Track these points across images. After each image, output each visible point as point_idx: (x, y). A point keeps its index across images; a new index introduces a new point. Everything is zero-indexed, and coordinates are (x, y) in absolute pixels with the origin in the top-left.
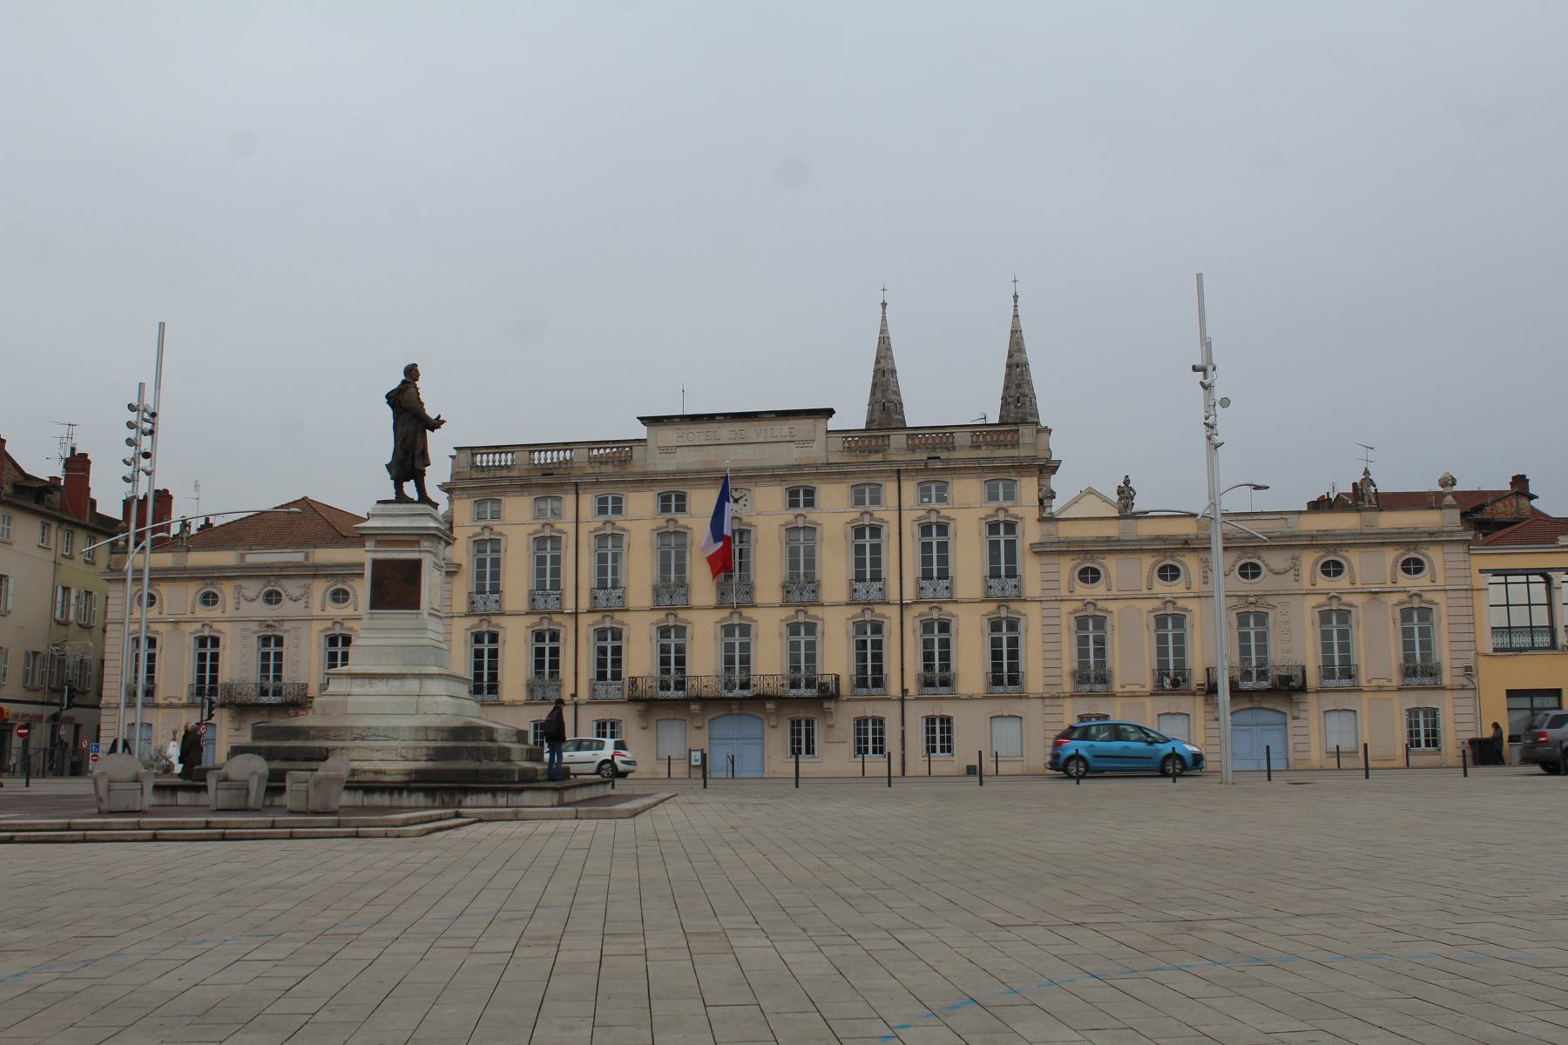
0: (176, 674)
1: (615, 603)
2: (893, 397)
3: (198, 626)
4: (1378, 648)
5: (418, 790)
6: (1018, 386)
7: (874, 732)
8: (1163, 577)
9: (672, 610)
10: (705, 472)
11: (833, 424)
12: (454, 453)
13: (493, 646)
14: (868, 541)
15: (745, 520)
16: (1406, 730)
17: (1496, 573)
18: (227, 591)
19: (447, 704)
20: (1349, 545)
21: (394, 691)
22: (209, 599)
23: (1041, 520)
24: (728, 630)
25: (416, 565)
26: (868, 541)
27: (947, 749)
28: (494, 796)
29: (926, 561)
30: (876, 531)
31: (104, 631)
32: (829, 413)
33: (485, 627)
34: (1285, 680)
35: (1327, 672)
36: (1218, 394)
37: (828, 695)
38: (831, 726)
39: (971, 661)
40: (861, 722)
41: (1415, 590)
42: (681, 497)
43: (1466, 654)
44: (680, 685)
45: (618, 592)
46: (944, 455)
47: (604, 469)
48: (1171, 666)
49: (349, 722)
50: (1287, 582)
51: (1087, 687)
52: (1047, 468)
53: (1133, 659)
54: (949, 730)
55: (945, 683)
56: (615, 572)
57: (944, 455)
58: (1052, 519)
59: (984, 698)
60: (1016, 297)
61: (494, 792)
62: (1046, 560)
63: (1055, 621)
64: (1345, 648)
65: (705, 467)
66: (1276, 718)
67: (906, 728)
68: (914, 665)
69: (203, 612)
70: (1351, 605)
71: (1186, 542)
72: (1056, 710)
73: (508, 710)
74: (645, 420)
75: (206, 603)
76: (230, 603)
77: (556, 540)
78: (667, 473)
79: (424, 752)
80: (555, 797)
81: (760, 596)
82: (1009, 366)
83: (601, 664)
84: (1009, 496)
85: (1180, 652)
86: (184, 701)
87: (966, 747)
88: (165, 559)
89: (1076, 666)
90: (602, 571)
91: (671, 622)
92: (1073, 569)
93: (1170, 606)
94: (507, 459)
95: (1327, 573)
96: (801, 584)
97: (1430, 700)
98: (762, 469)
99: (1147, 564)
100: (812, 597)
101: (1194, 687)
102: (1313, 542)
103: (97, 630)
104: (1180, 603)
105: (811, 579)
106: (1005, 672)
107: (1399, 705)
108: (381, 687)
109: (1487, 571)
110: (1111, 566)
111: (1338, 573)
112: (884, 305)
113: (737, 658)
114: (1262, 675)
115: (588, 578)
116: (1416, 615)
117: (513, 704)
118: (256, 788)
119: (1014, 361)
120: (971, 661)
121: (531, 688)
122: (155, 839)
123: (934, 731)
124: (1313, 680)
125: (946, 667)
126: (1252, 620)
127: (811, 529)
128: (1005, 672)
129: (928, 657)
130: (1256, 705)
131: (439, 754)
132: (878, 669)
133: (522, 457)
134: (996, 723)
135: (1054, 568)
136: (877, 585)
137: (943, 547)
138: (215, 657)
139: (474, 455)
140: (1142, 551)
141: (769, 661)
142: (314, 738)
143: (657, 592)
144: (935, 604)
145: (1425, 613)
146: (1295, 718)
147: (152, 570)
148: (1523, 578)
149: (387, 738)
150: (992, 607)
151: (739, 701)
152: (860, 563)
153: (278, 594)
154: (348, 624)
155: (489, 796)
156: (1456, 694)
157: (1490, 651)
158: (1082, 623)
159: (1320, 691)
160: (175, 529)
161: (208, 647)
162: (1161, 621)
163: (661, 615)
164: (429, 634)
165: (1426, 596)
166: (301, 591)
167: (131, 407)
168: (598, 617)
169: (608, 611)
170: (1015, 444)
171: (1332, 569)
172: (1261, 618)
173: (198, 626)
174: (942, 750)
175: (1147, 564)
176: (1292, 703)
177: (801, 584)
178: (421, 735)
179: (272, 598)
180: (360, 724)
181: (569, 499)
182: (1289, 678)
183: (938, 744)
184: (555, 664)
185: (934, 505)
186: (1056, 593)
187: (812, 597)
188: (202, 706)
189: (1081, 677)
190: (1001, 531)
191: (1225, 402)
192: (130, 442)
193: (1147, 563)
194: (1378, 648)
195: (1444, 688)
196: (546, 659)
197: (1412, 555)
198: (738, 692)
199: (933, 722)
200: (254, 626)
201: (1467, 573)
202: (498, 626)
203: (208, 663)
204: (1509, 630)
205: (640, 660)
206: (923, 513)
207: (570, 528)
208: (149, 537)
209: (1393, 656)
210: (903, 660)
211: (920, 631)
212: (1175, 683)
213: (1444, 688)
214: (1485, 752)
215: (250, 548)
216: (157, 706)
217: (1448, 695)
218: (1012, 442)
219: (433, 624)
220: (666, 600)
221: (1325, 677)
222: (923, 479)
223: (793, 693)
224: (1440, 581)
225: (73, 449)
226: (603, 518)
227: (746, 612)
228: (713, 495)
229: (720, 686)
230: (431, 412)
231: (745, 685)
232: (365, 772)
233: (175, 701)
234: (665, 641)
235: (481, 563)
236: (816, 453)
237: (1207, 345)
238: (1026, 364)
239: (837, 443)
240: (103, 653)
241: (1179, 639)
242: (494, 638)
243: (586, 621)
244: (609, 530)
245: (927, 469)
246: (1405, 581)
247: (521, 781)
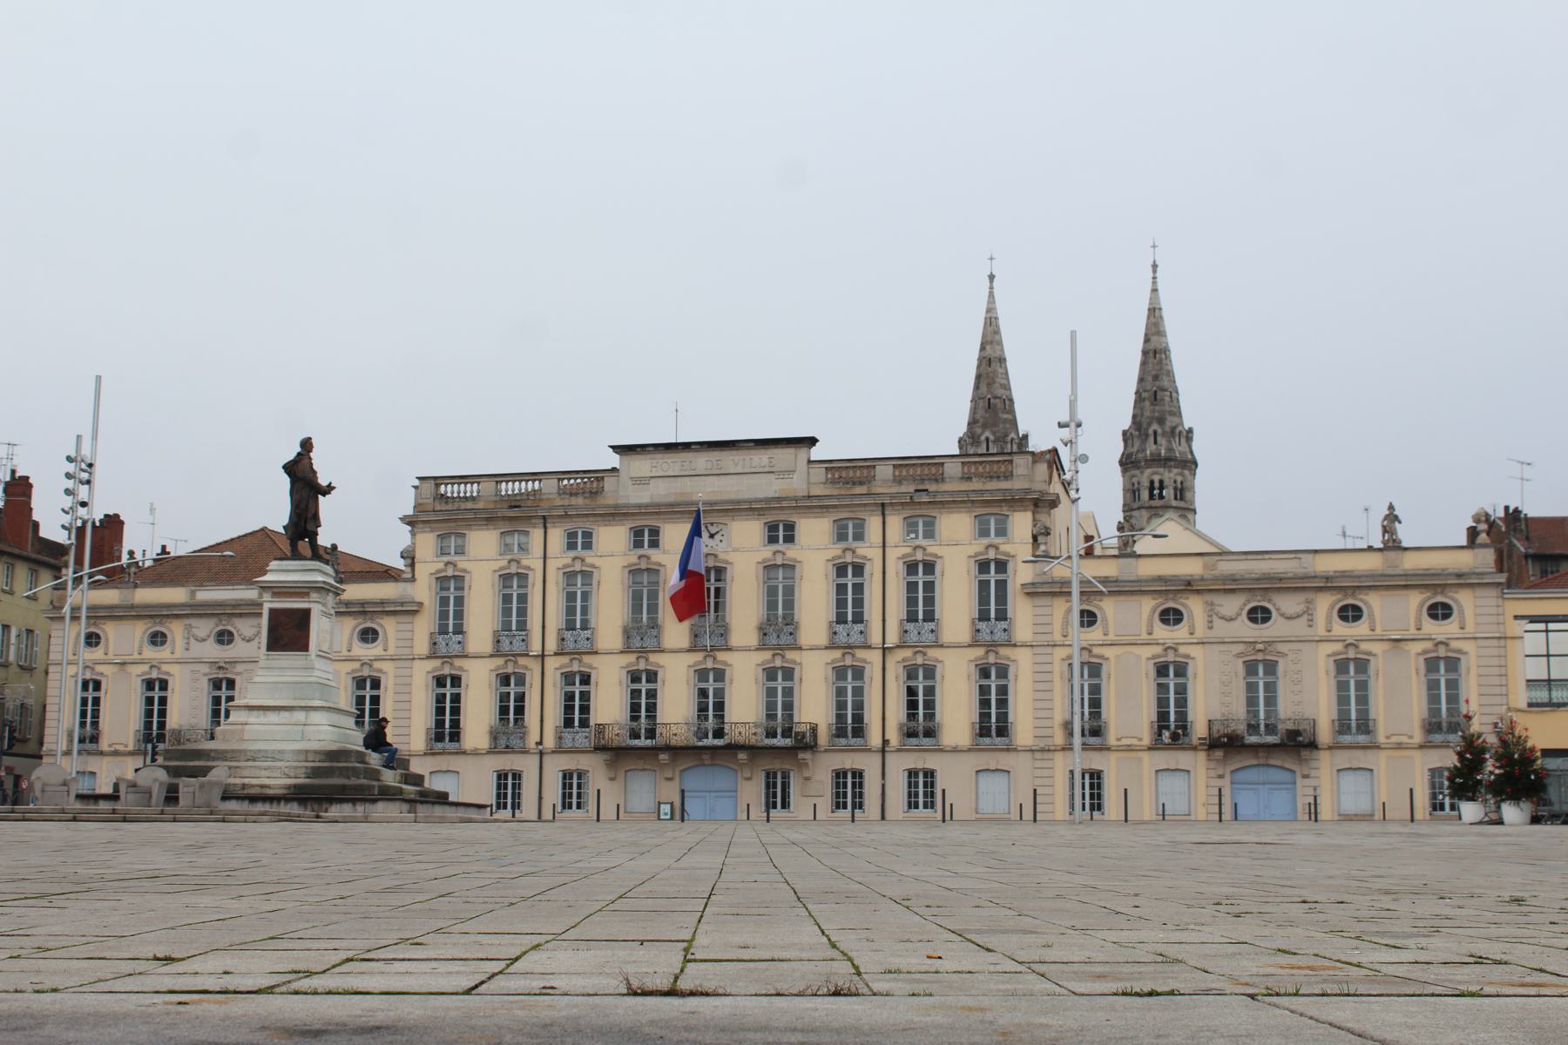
0: (122, 718)
2: (1000, 392)
3: (146, 668)
4: (1399, 703)
6: (1156, 378)
7: (925, 785)
9: (643, 652)
10: (678, 505)
11: (816, 453)
12: (417, 483)
14: (850, 580)
15: (722, 556)
17: (1534, 619)
18: (176, 630)
20: (1370, 588)
22: (158, 639)
25: (305, 615)
26: (850, 580)
29: (911, 602)
30: (859, 569)
31: (47, 673)
32: (812, 441)
34: (1293, 734)
35: (1342, 726)
37: (805, 744)
38: (808, 779)
39: (956, 712)
40: (840, 775)
41: (1441, 638)
42: (655, 532)
45: (587, 633)
46: (932, 487)
49: (244, 746)
50: (1299, 628)
55: (930, 733)
57: (932, 487)
59: (969, 750)
60: (1155, 266)
61: (354, 801)
62: (1040, 601)
63: (1048, 668)
65: (679, 499)
66: (1285, 776)
67: (887, 779)
69: (150, 653)
70: (1370, 654)
71: (1189, 583)
72: (1045, 764)
73: (470, 759)
74: (615, 448)
75: (154, 643)
76: (180, 643)
77: (522, 577)
78: (640, 506)
81: (736, 639)
83: (569, 709)
84: (1002, 532)
86: (131, 748)
88: (110, 596)
90: (570, 611)
92: (1332, 607)
93: (1171, 652)
94: (472, 489)
96: (779, 626)
98: (739, 502)
100: (789, 639)
101: (1195, 742)
103: (39, 673)
105: (789, 620)
106: (993, 724)
108: (273, 717)
111: (1357, 618)
112: (992, 277)
113: (710, 704)
114: (1271, 729)
117: (475, 753)
118: (158, 794)
119: (1152, 346)
120: (956, 712)
121: (494, 736)
122: (75, 819)
125: (930, 716)
126: (1261, 668)
127: (789, 567)
128: (993, 724)
130: (1262, 761)
131: (315, 772)
132: (858, 718)
133: (488, 487)
134: (983, 778)
135: (1047, 611)
136: (859, 627)
137: (930, 586)
138: (163, 701)
139: (437, 486)
141: (745, 708)
143: (627, 634)
144: (920, 648)
145: (1453, 664)
146: (1305, 777)
147: (91, 608)
149: (274, 759)
150: (980, 652)
151: (713, 749)
152: (841, 603)
153: (231, 634)
157: (1523, 705)
160: (125, 559)
161: (155, 689)
162: (1162, 670)
163: (632, 658)
164: (317, 673)
166: (1302, 607)
167: (69, 459)
169: (577, 654)
170: (1008, 476)
171: (1351, 613)
172: (1271, 668)
173: (146, 668)
174: (925, 807)
175: (1147, 606)
176: (1301, 761)
177: (779, 626)
178: (302, 757)
179: (1259, 615)
181: (537, 534)
182: (1296, 733)
183: (921, 800)
184: (520, 710)
185: (921, 541)
186: (1048, 637)
187: (789, 639)
188: (145, 754)
192: (68, 492)
196: (511, 709)
197: (1440, 599)
198: (710, 741)
199: (916, 775)
200: (205, 669)
202: (461, 669)
203: (156, 707)
205: (609, 706)
206: (909, 550)
208: (86, 580)
210: (885, 710)
211: (903, 677)
212: (1175, 737)
215: (201, 584)
216: (102, 753)
219: (320, 664)
220: (637, 643)
224: (1470, 629)
225: (13, 472)
226: (572, 554)
227: (721, 656)
228: (685, 529)
229: (625, 733)
230: (323, 481)
233: (121, 748)
235: (444, 601)
236: (797, 484)
239: (819, 474)
240: (45, 696)
243: (552, 664)
244: (578, 567)
245: (912, 503)
246: (1432, 628)
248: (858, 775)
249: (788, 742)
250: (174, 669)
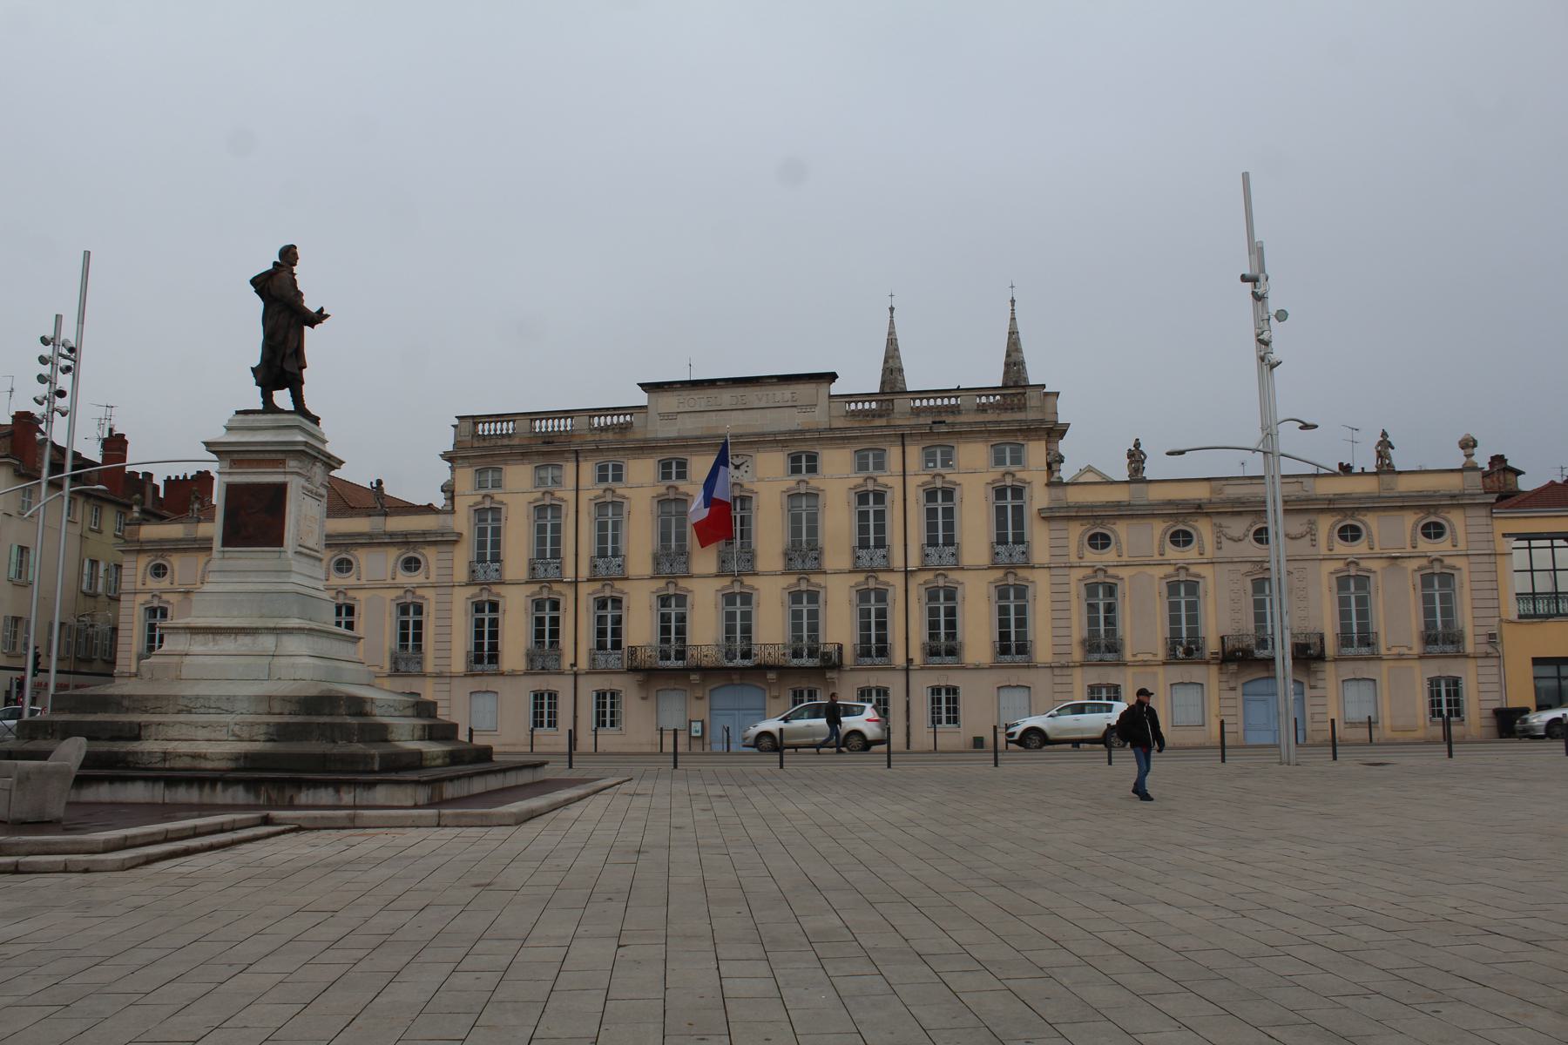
1: (615, 572)
4: (1397, 615)
5: (236, 782)
8: (1175, 543)
9: (672, 578)
11: (836, 388)
12: (456, 422)
13: (493, 615)
14: (871, 507)
15: (747, 486)
16: (1427, 700)
17: (1520, 537)
19: (301, 666)
21: (243, 650)
23: (1049, 484)
24: (730, 599)
25: (281, 489)
26: (871, 507)
27: (954, 719)
28: (338, 791)
29: (931, 527)
30: (880, 497)
32: (832, 377)
33: (485, 597)
35: (1345, 639)
36: (1273, 306)
37: (831, 664)
41: (1435, 555)
43: (1490, 621)
44: (681, 655)
45: (618, 560)
46: (950, 419)
47: (604, 436)
48: (1184, 634)
51: (1097, 656)
52: (1056, 432)
53: (1143, 626)
54: (535, 714)
55: (952, 652)
56: (615, 539)
58: (1060, 484)
59: (991, 668)
60: (1013, 301)
61: (337, 785)
62: (1055, 525)
63: (1065, 588)
64: (1363, 615)
68: (919, 634)
70: (1369, 571)
71: (1199, 506)
72: (1064, 680)
77: (556, 509)
78: (668, 440)
79: (263, 729)
80: (422, 795)
81: (762, 565)
82: (1007, 364)
83: (601, 633)
84: (1017, 460)
85: (1193, 619)
87: (977, 716)
89: (1085, 634)
90: (602, 539)
91: (672, 591)
92: (1082, 535)
95: (1344, 538)
96: (803, 552)
97: (1452, 668)
98: (763, 434)
99: (1158, 529)
101: (1208, 656)
102: (1330, 506)
104: (1193, 569)
106: (1012, 643)
107: (1419, 676)
108: (228, 644)
109: (1510, 535)
110: (1121, 531)
111: (1356, 538)
112: (892, 309)
115: (588, 547)
116: (1438, 580)
117: (513, 674)
121: (531, 658)
123: (939, 701)
124: (1330, 649)
125: (951, 636)
127: (813, 496)
128: (1012, 643)
129: (933, 625)
131: (282, 732)
132: (882, 639)
133: (523, 424)
134: (1005, 694)
136: (881, 552)
137: (949, 513)
139: (476, 424)
140: (1154, 516)
141: (771, 629)
142: (127, 710)
143: (657, 560)
145: (1447, 579)
148: (1547, 543)
149: (220, 711)
150: (999, 574)
151: (741, 671)
152: (863, 529)
154: (351, 593)
155: (331, 791)
156: (1480, 662)
157: (1514, 617)
158: (1091, 590)
159: (1338, 659)
162: (1173, 588)
163: (661, 583)
165: (1447, 561)
167: (45, 341)
168: (598, 585)
169: (609, 580)
170: (1022, 408)
171: (1350, 533)
174: (948, 721)
175: (1158, 529)
177: (803, 552)
178: (264, 707)
180: (187, 693)
181: (569, 468)
182: (1306, 647)
184: (555, 633)
185: (939, 470)
189: (1091, 645)
190: (1008, 496)
191: (1282, 316)
192: (42, 379)
193: (1159, 528)
194: (1397, 615)
195: (1467, 656)
196: (546, 631)
197: (1433, 519)
198: (738, 662)
199: (939, 692)
201: (1490, 537)
202: (498, 595)
204: (1534, 596)
205: (640, 630)
206: (928, 478)
207: (570, 496)
209: (1414, 623)
210: (908, 629)
211: (925, 599)
212: (1188, 652)
213: (1467, 656)
214: (1508, 723)
217: (1471, 663)
218: (1016, 411)
219: (300, 565)
220: (666, 569)
221: (1343, 645)
222: (928, 443)
223: (795, 662)
224: (1462, 545)
226: (603, 486)
227: (748, 581)
230: (311, 305)
231: (746, 655)
232: (179, 756)
234: (665, 610)
235: (482, 532)
236: (819, 417)
237: (1257, 251)
238: (1022, 363)
241: (1192, 607)
242: (494, 607)
243: (585, 589)
244: (609, 498)
245: (931, 433)
246: (1425, 545)
247: (381, 771)
248: (553, 696)
249: (815, 662)
250: (430, 594)
